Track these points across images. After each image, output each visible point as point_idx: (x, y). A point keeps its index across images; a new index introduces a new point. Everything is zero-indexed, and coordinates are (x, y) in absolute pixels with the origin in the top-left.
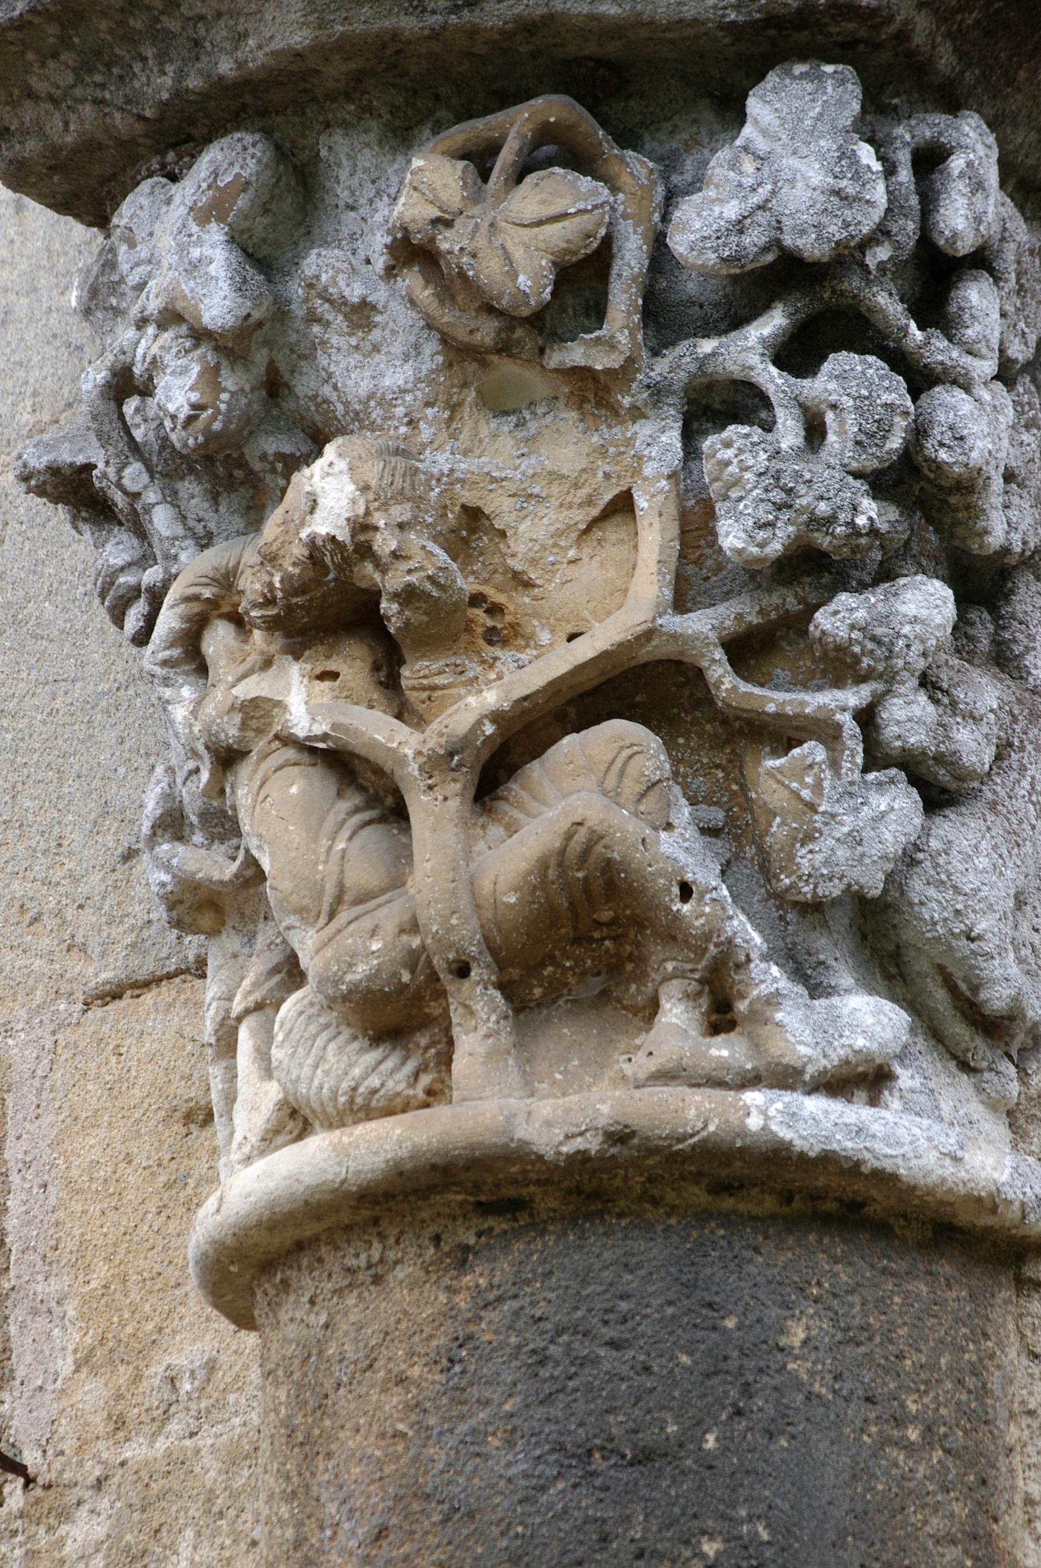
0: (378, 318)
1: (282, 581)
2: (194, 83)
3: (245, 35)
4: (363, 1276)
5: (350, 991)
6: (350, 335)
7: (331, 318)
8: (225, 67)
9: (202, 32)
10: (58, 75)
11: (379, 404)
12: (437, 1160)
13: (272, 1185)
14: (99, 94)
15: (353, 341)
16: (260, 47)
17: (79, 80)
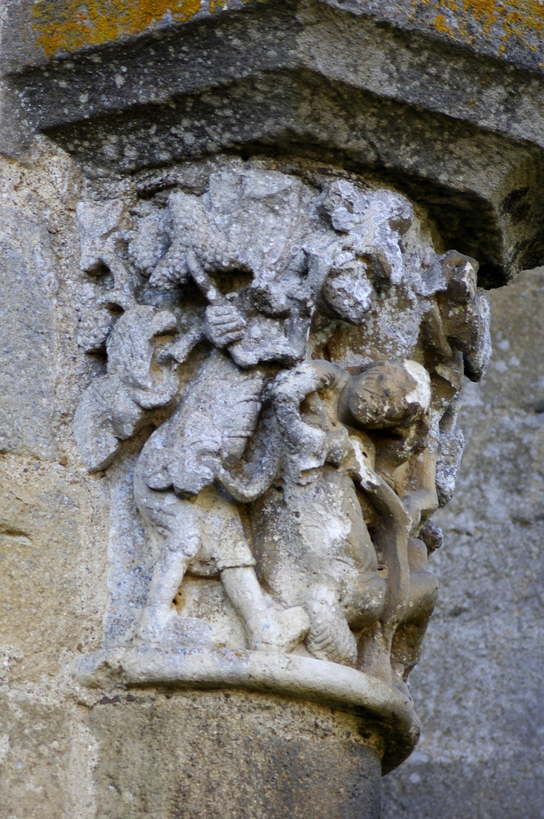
0: (408, 310)
1: (388, 410)
2: (423, 172)
3: (462, 173)
4: (319, 732)
5: (368, 609)
6: (394, 307)
7: (392, 295)
8: (443, 178)
9: (446, 158)
10: (371, 123)
11: (393, 344)
12: (396, 713)
13: (335, 679)
14: (375, 142)
15: (393, 310)
16: (464, 182)
17: (375, 131)
